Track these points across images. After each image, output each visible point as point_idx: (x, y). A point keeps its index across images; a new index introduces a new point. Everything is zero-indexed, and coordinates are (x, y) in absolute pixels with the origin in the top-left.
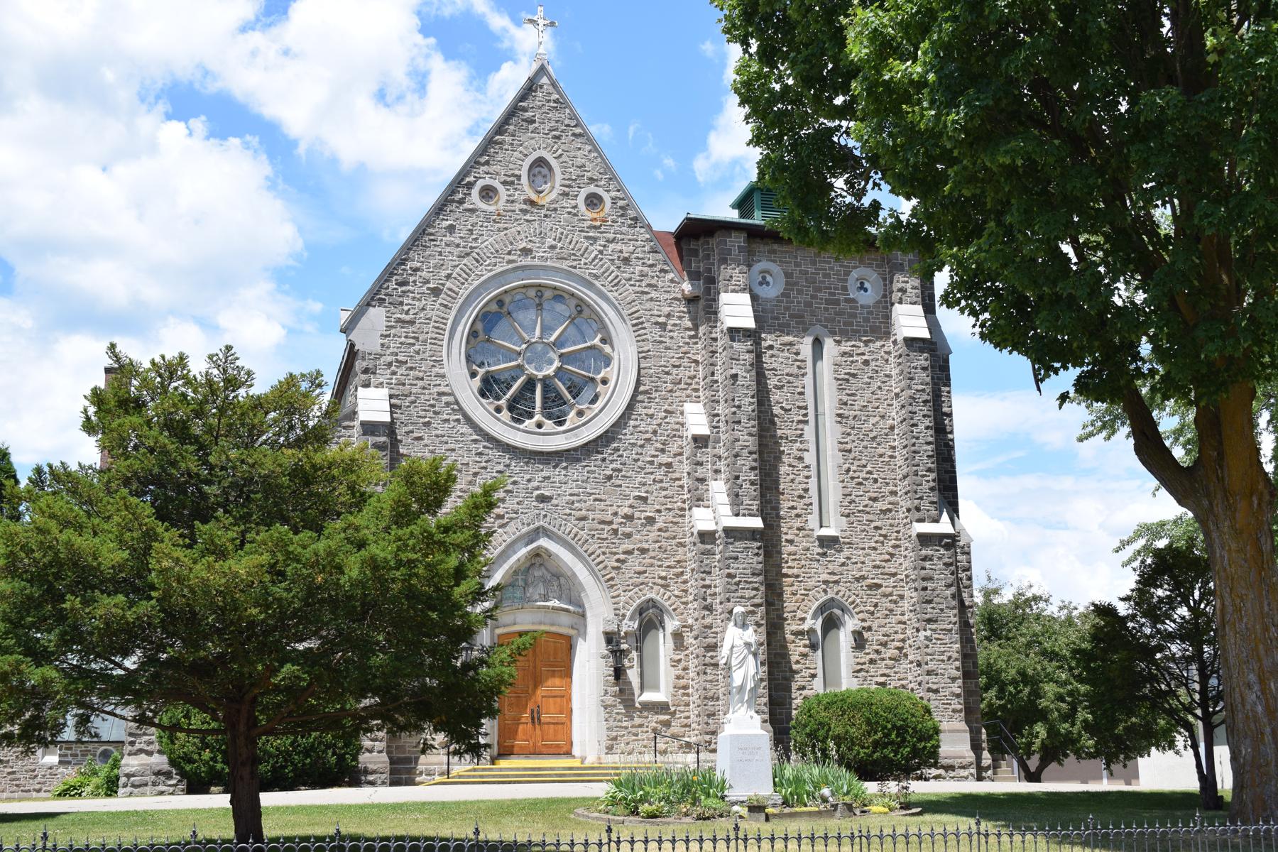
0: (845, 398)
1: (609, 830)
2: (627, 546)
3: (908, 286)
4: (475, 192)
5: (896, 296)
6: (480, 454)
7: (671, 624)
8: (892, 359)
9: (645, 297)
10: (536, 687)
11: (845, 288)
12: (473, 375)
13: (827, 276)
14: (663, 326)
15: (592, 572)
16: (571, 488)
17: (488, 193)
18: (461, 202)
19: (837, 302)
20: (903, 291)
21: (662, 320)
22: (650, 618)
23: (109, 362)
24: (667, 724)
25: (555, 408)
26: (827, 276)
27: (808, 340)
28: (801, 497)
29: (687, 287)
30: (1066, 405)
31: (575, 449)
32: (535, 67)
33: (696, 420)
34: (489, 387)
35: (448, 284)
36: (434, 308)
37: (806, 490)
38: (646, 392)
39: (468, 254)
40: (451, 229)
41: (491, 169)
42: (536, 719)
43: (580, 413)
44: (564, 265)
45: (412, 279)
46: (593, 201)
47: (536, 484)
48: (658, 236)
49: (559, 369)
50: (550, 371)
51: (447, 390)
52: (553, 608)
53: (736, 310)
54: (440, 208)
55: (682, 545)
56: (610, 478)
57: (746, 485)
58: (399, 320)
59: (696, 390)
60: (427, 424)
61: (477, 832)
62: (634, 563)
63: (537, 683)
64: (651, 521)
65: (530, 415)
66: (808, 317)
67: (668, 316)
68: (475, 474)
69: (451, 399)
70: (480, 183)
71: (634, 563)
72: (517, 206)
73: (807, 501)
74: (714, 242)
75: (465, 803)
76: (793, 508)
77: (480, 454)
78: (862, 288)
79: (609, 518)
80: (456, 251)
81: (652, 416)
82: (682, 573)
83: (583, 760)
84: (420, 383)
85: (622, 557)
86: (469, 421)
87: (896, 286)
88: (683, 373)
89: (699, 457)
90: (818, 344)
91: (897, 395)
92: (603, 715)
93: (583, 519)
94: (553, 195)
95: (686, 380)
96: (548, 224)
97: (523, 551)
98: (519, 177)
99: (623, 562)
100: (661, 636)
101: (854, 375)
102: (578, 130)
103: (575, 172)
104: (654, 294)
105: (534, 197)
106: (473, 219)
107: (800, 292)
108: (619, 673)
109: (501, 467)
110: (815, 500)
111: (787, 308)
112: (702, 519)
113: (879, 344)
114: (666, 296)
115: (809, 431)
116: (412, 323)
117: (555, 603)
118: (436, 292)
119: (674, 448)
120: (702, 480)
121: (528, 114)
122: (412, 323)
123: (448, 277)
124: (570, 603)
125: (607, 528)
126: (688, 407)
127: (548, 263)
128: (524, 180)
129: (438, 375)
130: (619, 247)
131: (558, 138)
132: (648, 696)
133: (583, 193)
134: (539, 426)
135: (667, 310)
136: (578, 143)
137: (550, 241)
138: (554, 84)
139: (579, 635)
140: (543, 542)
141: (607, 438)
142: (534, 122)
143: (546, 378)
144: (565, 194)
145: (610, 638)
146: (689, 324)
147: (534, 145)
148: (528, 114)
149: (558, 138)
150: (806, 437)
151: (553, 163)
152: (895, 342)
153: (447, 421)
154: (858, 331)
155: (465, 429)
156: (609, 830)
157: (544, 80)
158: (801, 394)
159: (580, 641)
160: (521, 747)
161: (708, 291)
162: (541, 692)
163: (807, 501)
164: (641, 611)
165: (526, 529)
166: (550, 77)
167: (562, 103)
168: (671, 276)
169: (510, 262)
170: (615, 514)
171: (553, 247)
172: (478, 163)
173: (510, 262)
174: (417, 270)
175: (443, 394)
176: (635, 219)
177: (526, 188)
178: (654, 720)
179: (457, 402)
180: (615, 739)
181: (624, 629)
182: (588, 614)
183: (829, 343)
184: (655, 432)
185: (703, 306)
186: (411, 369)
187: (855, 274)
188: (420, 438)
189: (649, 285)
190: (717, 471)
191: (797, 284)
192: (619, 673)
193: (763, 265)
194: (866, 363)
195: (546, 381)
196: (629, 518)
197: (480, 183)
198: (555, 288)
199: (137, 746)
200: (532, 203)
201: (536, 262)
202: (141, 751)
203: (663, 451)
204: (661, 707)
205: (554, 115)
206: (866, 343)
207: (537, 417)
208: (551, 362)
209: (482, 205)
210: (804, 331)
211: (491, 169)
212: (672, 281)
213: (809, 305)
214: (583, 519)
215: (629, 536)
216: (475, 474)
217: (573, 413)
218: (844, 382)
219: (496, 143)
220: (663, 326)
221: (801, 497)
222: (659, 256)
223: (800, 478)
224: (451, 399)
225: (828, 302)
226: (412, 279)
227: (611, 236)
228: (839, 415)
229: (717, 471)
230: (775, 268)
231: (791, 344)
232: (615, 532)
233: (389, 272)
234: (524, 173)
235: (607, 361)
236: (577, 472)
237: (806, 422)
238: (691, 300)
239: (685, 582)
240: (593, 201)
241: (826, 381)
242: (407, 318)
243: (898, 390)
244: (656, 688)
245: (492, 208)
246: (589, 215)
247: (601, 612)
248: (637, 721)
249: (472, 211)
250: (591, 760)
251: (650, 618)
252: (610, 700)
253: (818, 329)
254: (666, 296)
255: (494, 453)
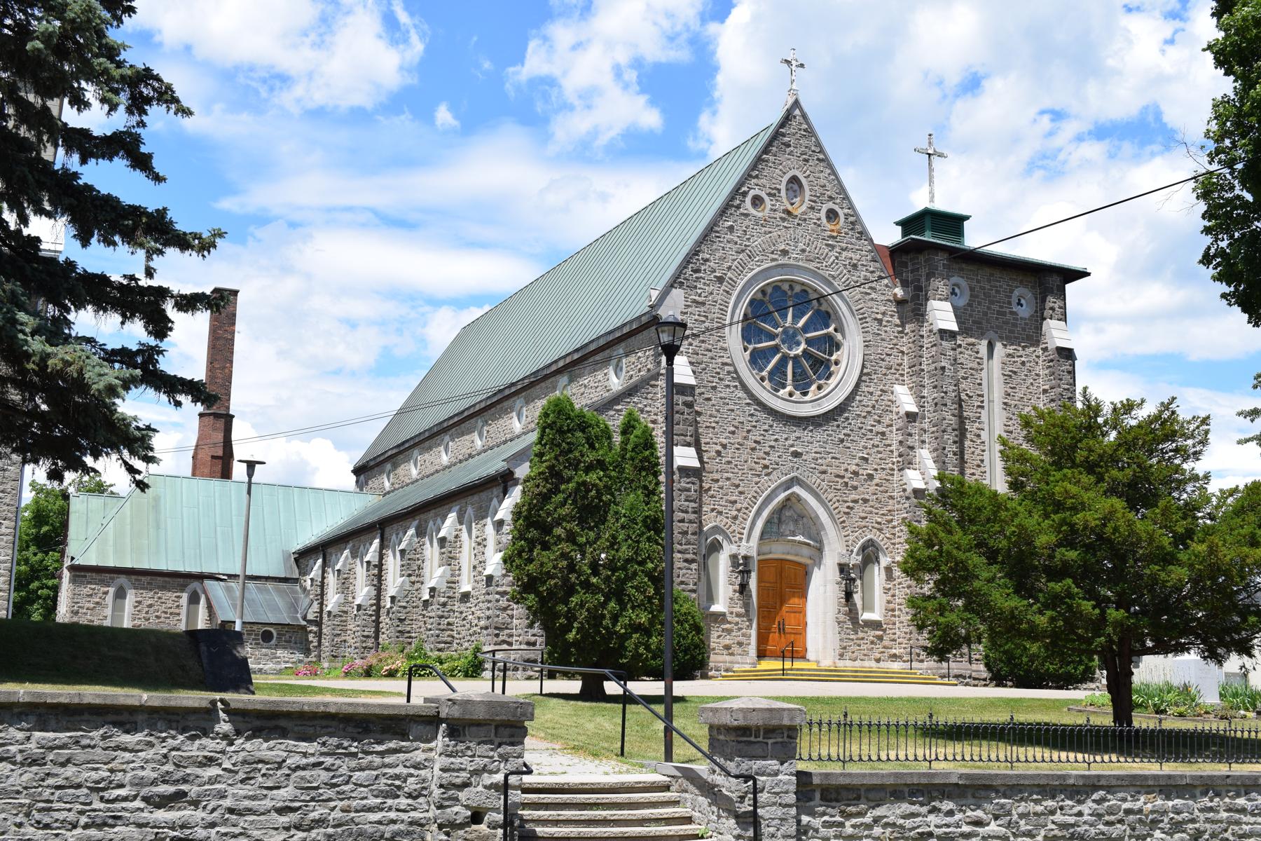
0: (1009, 391)
1: (846, 716)
2: (854, 496)
3: (1056, 306)
4: (748, 199)
5: (1047, 313)
6: (752, 415)
7: (885, 561)
8: (1040, 362)
9: (868, 297)
10: (781, 605)
11: (1010, 303)
12: (746, 349)
13: (998, 292)
14: (880, 321)
15: (831, 516)
16: (815, 447)
17: (757, 201)
18: (738, 207)
19: (1004, 314)
20: (1052, 309)
21: (879, 316)
22: (870, 553)
23: (1166, 401)
24: (880, 638)
25: (802, 384)
26: (998, 292)
27: (985, 343)
28: (979, 466)
29: (899, 292)
30: (1203, 415)
31: (818, 416)
32: (791, 101)
33: (906, 400)
34: (757, 359)
35: (729, 274)
36: (718, 292)
37: (982, 461)
38: (868, 374)
39: (743, 251)
40: (731, 228)
41: (760, 182)
42: (782, 630)
43: (819, 388)
44: (811, 266)
45: (703, 268)
46: (832, 215)
47: (791, 442)
48: (877, 249)
49: (804, 351)
50: (799, 351)
51: (729, 361)
52: (800, 542)
53: (942, 314)
54: (723, 211)
55: (892, 498)
56: (842, 441)
57: (950, 455)
58: (694, 301)
59: (902, 375)
60: (714, 388)
61: (1088, 720)
62: (859, 509)
63: (783, 602)
64: (871, 477)
65: (784, 386)
66: (984, 324)
67: (884, 314)
68: (749, 431)
69: (731, 369)
70: (752, 193)
71: (859, 509)
72: (778, 215)
73: (982, 469)
74: (922, 258)
75: (966, 699)
76: (973, 474)
77: (752, 415)
78: (1019, 304)
79: (842, 473)
80: (735, 247)
81: (871, 394)
82: (892, 520)
83: (818, 662)
84: (709, 354)
85: (851, 504)
86: (744, 387)
87: (1049, 304)
88: (893, 361)
89: (910, 429)
90: (991, 347)
91: (1045, 391)
92: (837, 629)
93: (824, 472)
94: (804, 208)
95: (895, 366)
96: (800, 231)
97: (782, 496)
98: (779, 190)
99: (852, 508)
100: (876, 568)
101: (1015, 373)
102: (821, 156)
103: (819, 191)
104: (873, 295)
105: (790, 208)
106: (747, 222)
107: (979, 303)
108: (849, 595)
109: (766, 427)
110: (987, 469)
111: (971, 316)
112: (914, 479)
113: (1032, 349)
114: (882, 298)
115: (984, 413)
116: (703, 304)
117: (800, 538)
118: (720, 280)
119: (886, 421)
120: (912, 448)
121: (786, 139)
122: (703, 304)
123: (729, 268)
124: (810, 538)
125: (840, 481)
126: (899, 389)
127: (800, 263)
128: (783, 193)
129: (722, 349)
130: (850, 254)
131: (807, 161)
132: (867, 616)
133: (825, 208)
134: (791, 395)
135: (883, 309)
136: (821, 166)
137: (801, 246)
138: (804, 116)
139: (815, 564)
140: (796, 489)
141: (841, 409)
142: (789, 146)
143: (796, 357)
144: (812, 208)
145: (843, 568)
146: (898, 322)
147: (788, 165)
148: (786, 139)
149: (807, 161)
150: (983, 419)
151: (804, 181)
152: (1045, 350)
153: (728, 386)
154: (1017, 338)
155: (741, 394)
156: (846, 716)
157: (797, 112)
158: (980, 384)
159: (816, 569)
160: (771, 651)
161: (916, 297)
162: (784, 609)
163: (982, 469)
164: (864, 548)
165: (784, 478)
166: (801, 110)
167: (810, 132)
168: (886, 281)
169: (773, 260)
170: (846, 470)
171: (803, 251)
172: (750, 176)
173: (773, 260)
174: (707, 260)
175: (726, 364)
176: (861, 233)
177: (785, 200)
178: (872, 633)
179: (736, 372)
180: (845, 648)
181: (852, 562)
182: (826, 548)
183: (998, 347)
184: (874, 407)
185: (912, 309)
186: (703, 342)
187: (1016, 293)
188: (709, 399)
189: (871, 288)
190: (923, 442)
191: (977, 297)
192: (849, 595)
193: (955, 279)
194: (1023, 363)
195: (796, 358)
196: (856, 473)
197: (752, 193)
198: (803, 284)
199: (501, 638)
200: (789, 213)
201: (792, 262)
202: (504, 642)
203: (879, 422)
204: (876, 625)
205: (803, 142)
206: (1024, 348)
207: (789, 388)
208: (798, 344)
209: (753, 211)
210: (981, 336)
211: (760, 182)
212: (887, 286)
213: (985, 314)
214: (824, 472)
215: (855, 488)
216: (749, 431)
217: (814, 387)
218: (1009, 377)
219: (764, 160)
220: (880, 321)
221: (979, 466)
222: (878, 265)
223: (978, 452)
224: (731, 369)
225: (999, 313)
226: (703, 268)
227: (844, 245)
228: (1005, 404)
229: (923, 442)
230: (963, 283)
231: (973, 345)
232: (846, 484)
233: (687, 261)
234: (783, 187)
235: (838, 346)
236: (819, 435)
237: (982, 407)
238: (900, 303)
239: (894, 527)
240: (832, 215)
241: (995, 375)
242: (700, 299)
243: (1047, 387)
244: (872, 610)
245: (760, 215)
246: (829, 226)
247: (836, 549)
248: (861, 635)
249: (746, 215)
250: (827, 663)
251: (870, 553)
252: (842, 618)
253: (991, 334)
254: (882, 298)
255: (761, 415)
